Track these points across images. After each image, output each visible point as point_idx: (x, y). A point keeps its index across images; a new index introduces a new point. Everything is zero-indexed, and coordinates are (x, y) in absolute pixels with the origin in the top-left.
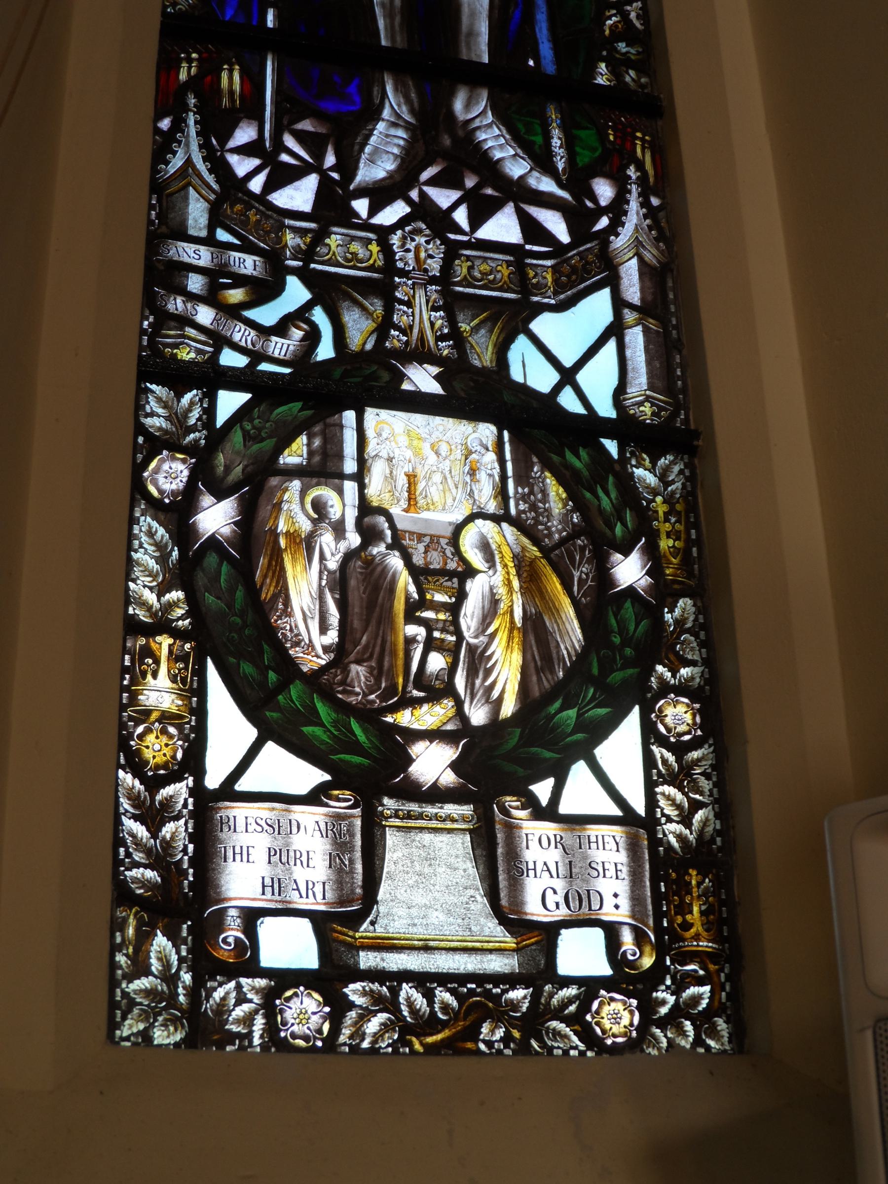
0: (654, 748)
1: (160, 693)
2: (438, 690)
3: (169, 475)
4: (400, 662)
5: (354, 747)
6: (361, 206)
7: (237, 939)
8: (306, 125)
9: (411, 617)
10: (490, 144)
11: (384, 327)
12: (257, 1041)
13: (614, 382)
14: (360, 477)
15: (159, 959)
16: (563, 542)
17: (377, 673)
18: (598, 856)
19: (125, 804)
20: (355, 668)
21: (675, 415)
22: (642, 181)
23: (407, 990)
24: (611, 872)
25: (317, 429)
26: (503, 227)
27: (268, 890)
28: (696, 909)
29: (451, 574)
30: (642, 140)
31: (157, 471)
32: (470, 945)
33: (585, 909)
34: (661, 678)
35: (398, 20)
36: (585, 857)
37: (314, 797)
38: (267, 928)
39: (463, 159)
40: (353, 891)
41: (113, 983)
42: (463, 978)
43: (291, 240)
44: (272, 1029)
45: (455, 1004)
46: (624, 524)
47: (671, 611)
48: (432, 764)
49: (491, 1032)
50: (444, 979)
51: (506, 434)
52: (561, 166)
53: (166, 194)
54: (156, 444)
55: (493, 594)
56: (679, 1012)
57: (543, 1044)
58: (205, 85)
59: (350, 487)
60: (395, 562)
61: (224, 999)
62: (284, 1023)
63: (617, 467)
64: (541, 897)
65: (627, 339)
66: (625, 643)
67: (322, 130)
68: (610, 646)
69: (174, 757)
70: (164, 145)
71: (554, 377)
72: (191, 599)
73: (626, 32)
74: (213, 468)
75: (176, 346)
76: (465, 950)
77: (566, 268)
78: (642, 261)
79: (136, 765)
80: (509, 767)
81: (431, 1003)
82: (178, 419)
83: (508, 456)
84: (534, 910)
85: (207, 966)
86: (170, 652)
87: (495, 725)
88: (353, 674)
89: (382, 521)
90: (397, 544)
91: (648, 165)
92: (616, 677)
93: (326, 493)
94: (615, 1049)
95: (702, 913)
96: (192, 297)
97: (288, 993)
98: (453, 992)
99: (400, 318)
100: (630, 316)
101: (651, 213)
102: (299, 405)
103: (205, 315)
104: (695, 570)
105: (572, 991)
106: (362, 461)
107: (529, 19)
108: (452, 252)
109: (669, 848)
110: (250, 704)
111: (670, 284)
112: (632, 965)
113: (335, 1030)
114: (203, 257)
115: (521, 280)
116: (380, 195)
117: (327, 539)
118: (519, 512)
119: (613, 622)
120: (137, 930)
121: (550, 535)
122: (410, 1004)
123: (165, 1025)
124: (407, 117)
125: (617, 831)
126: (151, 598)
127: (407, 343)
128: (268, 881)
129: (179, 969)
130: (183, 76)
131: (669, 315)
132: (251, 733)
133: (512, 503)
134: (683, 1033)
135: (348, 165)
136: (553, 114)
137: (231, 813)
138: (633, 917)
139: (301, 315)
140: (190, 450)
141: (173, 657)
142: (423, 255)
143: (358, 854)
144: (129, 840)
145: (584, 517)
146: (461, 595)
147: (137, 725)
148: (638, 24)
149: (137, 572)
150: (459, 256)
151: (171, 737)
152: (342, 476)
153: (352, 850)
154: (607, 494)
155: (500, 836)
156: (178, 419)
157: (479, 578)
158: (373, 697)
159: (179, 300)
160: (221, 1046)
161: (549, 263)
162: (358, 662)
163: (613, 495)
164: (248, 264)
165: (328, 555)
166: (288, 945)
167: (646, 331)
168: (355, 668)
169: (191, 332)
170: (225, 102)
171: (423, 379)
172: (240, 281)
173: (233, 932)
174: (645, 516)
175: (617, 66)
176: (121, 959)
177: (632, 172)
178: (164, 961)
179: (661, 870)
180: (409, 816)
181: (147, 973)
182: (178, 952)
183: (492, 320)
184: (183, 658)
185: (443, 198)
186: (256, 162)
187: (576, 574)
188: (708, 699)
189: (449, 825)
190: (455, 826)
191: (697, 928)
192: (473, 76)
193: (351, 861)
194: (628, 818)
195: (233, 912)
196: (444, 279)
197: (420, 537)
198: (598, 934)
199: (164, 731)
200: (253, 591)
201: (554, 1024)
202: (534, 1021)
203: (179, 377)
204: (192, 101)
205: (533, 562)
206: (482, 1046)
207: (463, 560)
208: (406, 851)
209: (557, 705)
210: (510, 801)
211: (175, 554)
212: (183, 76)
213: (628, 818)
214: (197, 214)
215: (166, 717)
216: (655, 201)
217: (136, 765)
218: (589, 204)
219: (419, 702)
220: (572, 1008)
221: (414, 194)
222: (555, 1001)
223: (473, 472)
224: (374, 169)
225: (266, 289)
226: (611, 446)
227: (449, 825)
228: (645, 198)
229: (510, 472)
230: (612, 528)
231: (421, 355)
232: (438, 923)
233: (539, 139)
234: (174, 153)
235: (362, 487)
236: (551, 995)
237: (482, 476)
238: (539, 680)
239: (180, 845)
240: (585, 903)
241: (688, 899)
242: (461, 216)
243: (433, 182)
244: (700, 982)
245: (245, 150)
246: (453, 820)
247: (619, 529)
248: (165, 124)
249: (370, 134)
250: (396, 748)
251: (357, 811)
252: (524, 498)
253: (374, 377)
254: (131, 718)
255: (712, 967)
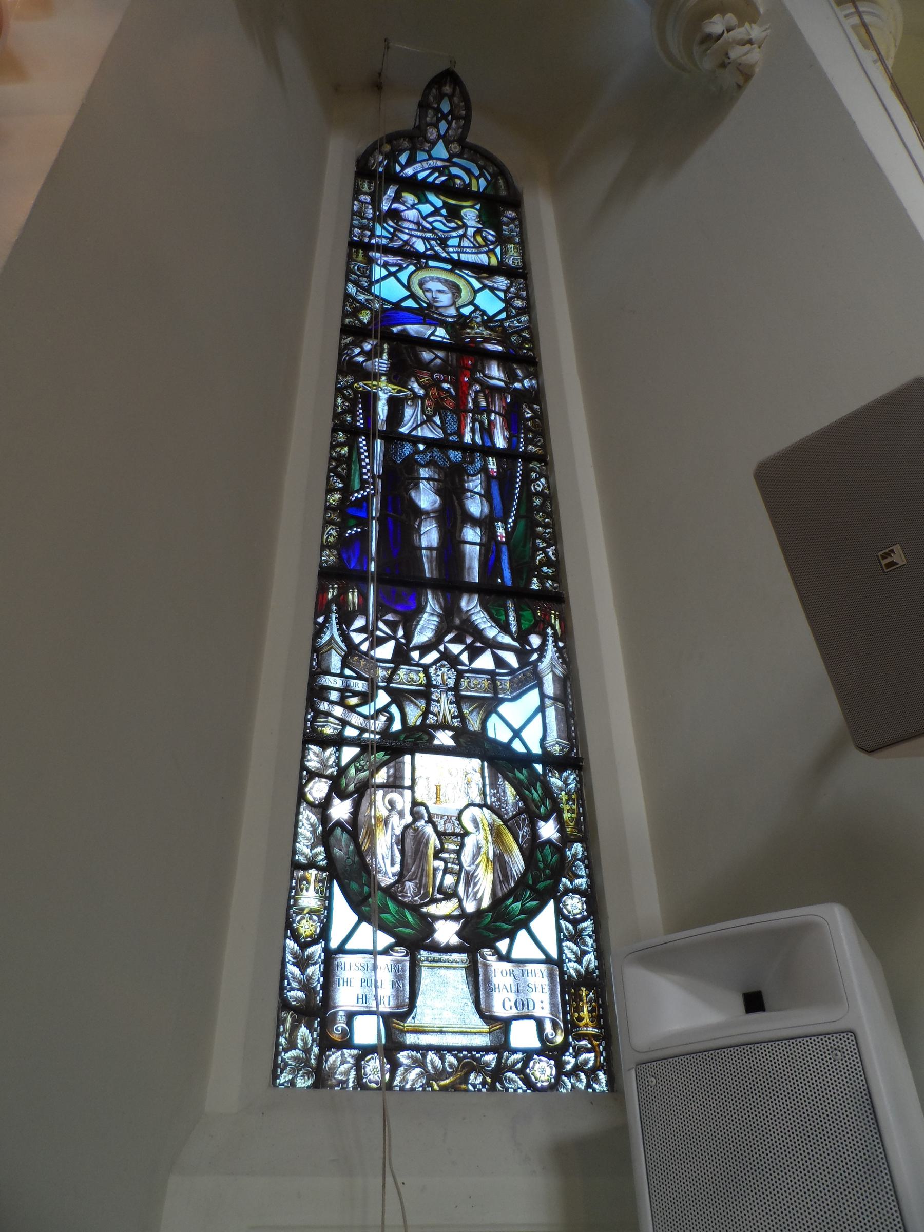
0: (561, 922)
1: (309, 899)
2: (449, 895)
3: (318, 789)
4: (431, 880)
5: (407, 925)
6: (415, 655)
7: (343, 1028)
8: (389, 617)
9: (436, 857)
10: (479, 621)
11: (426, 713)
12: (351, 1084)
13: (540, 735)
14: (412, 788)
15: (302, 1040)
16: (514, 817)
17: (419, 886)
18: (531, 980)
19: (289, 957)
20: (408, 883)
21: (571, 750)
22: (555, 635)
23: (431, 1056)
24: (539, 989)
25: (391, 764)
26: (485, 661)
27: (360, 1001)
28: (585, 1009)
29: (456, 835)
30: (555, 614)
31: (312, 788)
32: (464, 1030)
33: (525, 1010)
34: (565, 885)
35: (434, 563)
36: (525, 982)
37: (386, 952)
38: (358, 1021)
39: (468, 631)
40: (404, 1001)
41: (277, 1054)
42: (460, 1049)
43: (381, 673)
44: (359, 1077)
45: (456, 1063)
46: (545, 806)
47: (570, 850)
48: (446, 933)
49: (475, 1079)
50: (450, 1049)
51: (485, 763)
52: (514, 630)
53: (319, 652)
54: (313, 775)
55: (478, 844)
56: (577, 1068)
57: (503, 1086)
58: (341, 601)
59: (407, 793)
60: (429, 829)
61: (334, 1061)
62: (365, 1074)
63: (542, 778)
64: (502, 1005)
65: (547, 713)
66: (546, 867)
67: (397, 619)
68: (538, 868)
69: (315, 931)
70: (319, 630)
71: (511, 734)
72: (328, 852)
73: (548, 562)
74: (340, 785)
75: (324, 726)
76: (462, 1033)
77: (516, 680)
78: (554, 674)
79: (296, 937)
80: (486, 933)
81: (443, 1062)
82: (324, 763)
83: (486, 774)
84: (499, 1011)
85: (327, 1044)
86: (316, 878)
87: (479, 913)
88: (407, 887)
89: (422, 809)
90: (430, 821)
91: (558, 627)
92: (541, 885)
93: (394, 795)
94: (543, 1090)
95: (589, 1012)
96: (332, 703)
97: (368, 1058)
98: (455, 1056)
99: (434, 709)
100: (548, 702)
101: (559, 650)
102: (383, 753)
103: (338, 711)
104: (583, 830)
105: (519, 1056)
106: (413, 780)
107: (498, 559)
108: (460, 675)
109: (570, 976)
110: (356, 903)
111: (569, 685)
112: (551, 1041)
113: (392, 1077)
114: (338, 683)
115: (494, 688)
116: (425, 649)
117: (395, 820)
118: (492, 802)
119: (540, 856)
120: (292, 1024)
121: (507, 813)
122: (432, 1063)
123: (303, 1076)
124: (439, 611)
125: (543, 967)
126: (307, 851)
127: (437, 721)
128: (360, 997)
129: (312, 1045)
130: (330, 596)
131: (569, 701)
132: (355, 918)
133: (488, 798)
134: (580, 1080)
135: (409, 636)
136: (510, 604)
137: (343, 960)
138: (551, 1014)
139: (385, 709)
140: (328, 777)
141: (318, 880)
142: (445, 677)
143: (407, 981)
144: (290, 976)
145: (525, 804)
146: (462, 845)
147: (297, 915)
148: (553, 558)
149: (301, 838)
150: (463, 677)
151: (314, 921)
152: (403, 787)
153: (404, 979)
154: (537, 791)
155: (481, 971)
156: (324, 763)
157: (471, 836)
158: (416, 898)
159: (326, 703)
160: (332, 1087)
161: (507, 678)
162: (410, 881)
163: (540, 792)
164: (360, 686)
165: (395, 827)
166: (367, 1031)
167: (556, 709)
168: (408, 883)
169: (331, 719)
170: (350, 607)
171: (444, 738)
172: (355, 694)
173: (341, 1025)
174: (555, 802)
175: (542, 578)
176: (282, 1040)
177: (549, 631)
178: (305, 1042)
179: (568, 988)
180: (434, 960)
181: (295, 1048)
182: (312, 1036)
183: (479, 707)
184: (322, 881)
185: (456, 649)
186: (365, 636)
187: (521, 833)
188: (591, 896)
189: (455, 965)
190: (457, 965)
191: (587, 1020)
192: (471, 589)
193: (403, 985)
194: (548, 960)
195: (341, 1013)
196: (456, 688)
197: (442, 817)
198: (533, 1023)
199: (310, 918)
200: (358, 846)
201: (509, 1074)
202: (498, 1073)
203: (324, 742)
204: (334, 608)
205: (498, 828)
206: (470, 1087)
207: (463, 827)
208: (432, 979)
209: (511, 900)
210: (486, 951)
211: (320, 828)
212: (330, 596)
213: (548, 960)
214: (335, 662)
215: (312, 912)
216: (561, 644)
217: (296, 937)
218: (528, 648)
219: (440, 900)
220: (519, 1065)
221: (442, 648)
222: (509, 1062)
223: (468, 783)
224: (422, 636)
225: (366, 698)
226: (539, 768)
227: (455, 965)
228: (556, 642)
229: (487, 782)
230: (539, 809)
231: (444, 726)
232: (448, 1019)
233: (503, 618)
234: (325, 633)
235: (413, 792)
236: (508, 1058)
237: (473, 785)
238: (502, 887)
239: (316, 978)
240: (526, 1006)
241: (581, 1004)
242: (464, 657)
243: (451, 641)
244: (589, 1051)
245: (360, 630)
246: (457, 962)
247: (542, 809)
248: (321, 619)
249: (419, 621)
250: (427, 924)
251: (408, 958)
252: (494, 795)
253: (420, 738)
254: (294, 912)
255: (596, 1043)
